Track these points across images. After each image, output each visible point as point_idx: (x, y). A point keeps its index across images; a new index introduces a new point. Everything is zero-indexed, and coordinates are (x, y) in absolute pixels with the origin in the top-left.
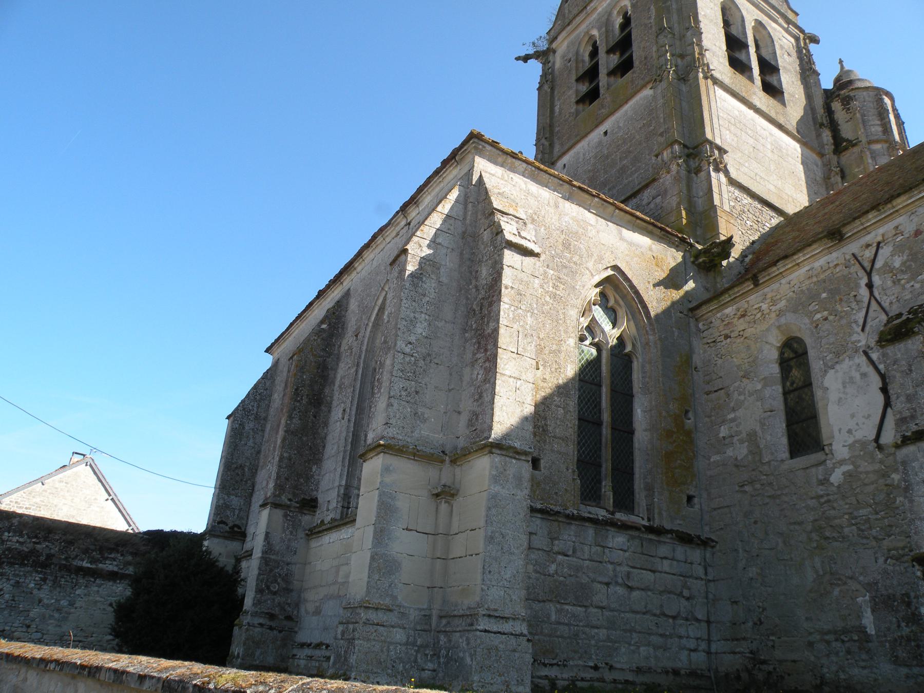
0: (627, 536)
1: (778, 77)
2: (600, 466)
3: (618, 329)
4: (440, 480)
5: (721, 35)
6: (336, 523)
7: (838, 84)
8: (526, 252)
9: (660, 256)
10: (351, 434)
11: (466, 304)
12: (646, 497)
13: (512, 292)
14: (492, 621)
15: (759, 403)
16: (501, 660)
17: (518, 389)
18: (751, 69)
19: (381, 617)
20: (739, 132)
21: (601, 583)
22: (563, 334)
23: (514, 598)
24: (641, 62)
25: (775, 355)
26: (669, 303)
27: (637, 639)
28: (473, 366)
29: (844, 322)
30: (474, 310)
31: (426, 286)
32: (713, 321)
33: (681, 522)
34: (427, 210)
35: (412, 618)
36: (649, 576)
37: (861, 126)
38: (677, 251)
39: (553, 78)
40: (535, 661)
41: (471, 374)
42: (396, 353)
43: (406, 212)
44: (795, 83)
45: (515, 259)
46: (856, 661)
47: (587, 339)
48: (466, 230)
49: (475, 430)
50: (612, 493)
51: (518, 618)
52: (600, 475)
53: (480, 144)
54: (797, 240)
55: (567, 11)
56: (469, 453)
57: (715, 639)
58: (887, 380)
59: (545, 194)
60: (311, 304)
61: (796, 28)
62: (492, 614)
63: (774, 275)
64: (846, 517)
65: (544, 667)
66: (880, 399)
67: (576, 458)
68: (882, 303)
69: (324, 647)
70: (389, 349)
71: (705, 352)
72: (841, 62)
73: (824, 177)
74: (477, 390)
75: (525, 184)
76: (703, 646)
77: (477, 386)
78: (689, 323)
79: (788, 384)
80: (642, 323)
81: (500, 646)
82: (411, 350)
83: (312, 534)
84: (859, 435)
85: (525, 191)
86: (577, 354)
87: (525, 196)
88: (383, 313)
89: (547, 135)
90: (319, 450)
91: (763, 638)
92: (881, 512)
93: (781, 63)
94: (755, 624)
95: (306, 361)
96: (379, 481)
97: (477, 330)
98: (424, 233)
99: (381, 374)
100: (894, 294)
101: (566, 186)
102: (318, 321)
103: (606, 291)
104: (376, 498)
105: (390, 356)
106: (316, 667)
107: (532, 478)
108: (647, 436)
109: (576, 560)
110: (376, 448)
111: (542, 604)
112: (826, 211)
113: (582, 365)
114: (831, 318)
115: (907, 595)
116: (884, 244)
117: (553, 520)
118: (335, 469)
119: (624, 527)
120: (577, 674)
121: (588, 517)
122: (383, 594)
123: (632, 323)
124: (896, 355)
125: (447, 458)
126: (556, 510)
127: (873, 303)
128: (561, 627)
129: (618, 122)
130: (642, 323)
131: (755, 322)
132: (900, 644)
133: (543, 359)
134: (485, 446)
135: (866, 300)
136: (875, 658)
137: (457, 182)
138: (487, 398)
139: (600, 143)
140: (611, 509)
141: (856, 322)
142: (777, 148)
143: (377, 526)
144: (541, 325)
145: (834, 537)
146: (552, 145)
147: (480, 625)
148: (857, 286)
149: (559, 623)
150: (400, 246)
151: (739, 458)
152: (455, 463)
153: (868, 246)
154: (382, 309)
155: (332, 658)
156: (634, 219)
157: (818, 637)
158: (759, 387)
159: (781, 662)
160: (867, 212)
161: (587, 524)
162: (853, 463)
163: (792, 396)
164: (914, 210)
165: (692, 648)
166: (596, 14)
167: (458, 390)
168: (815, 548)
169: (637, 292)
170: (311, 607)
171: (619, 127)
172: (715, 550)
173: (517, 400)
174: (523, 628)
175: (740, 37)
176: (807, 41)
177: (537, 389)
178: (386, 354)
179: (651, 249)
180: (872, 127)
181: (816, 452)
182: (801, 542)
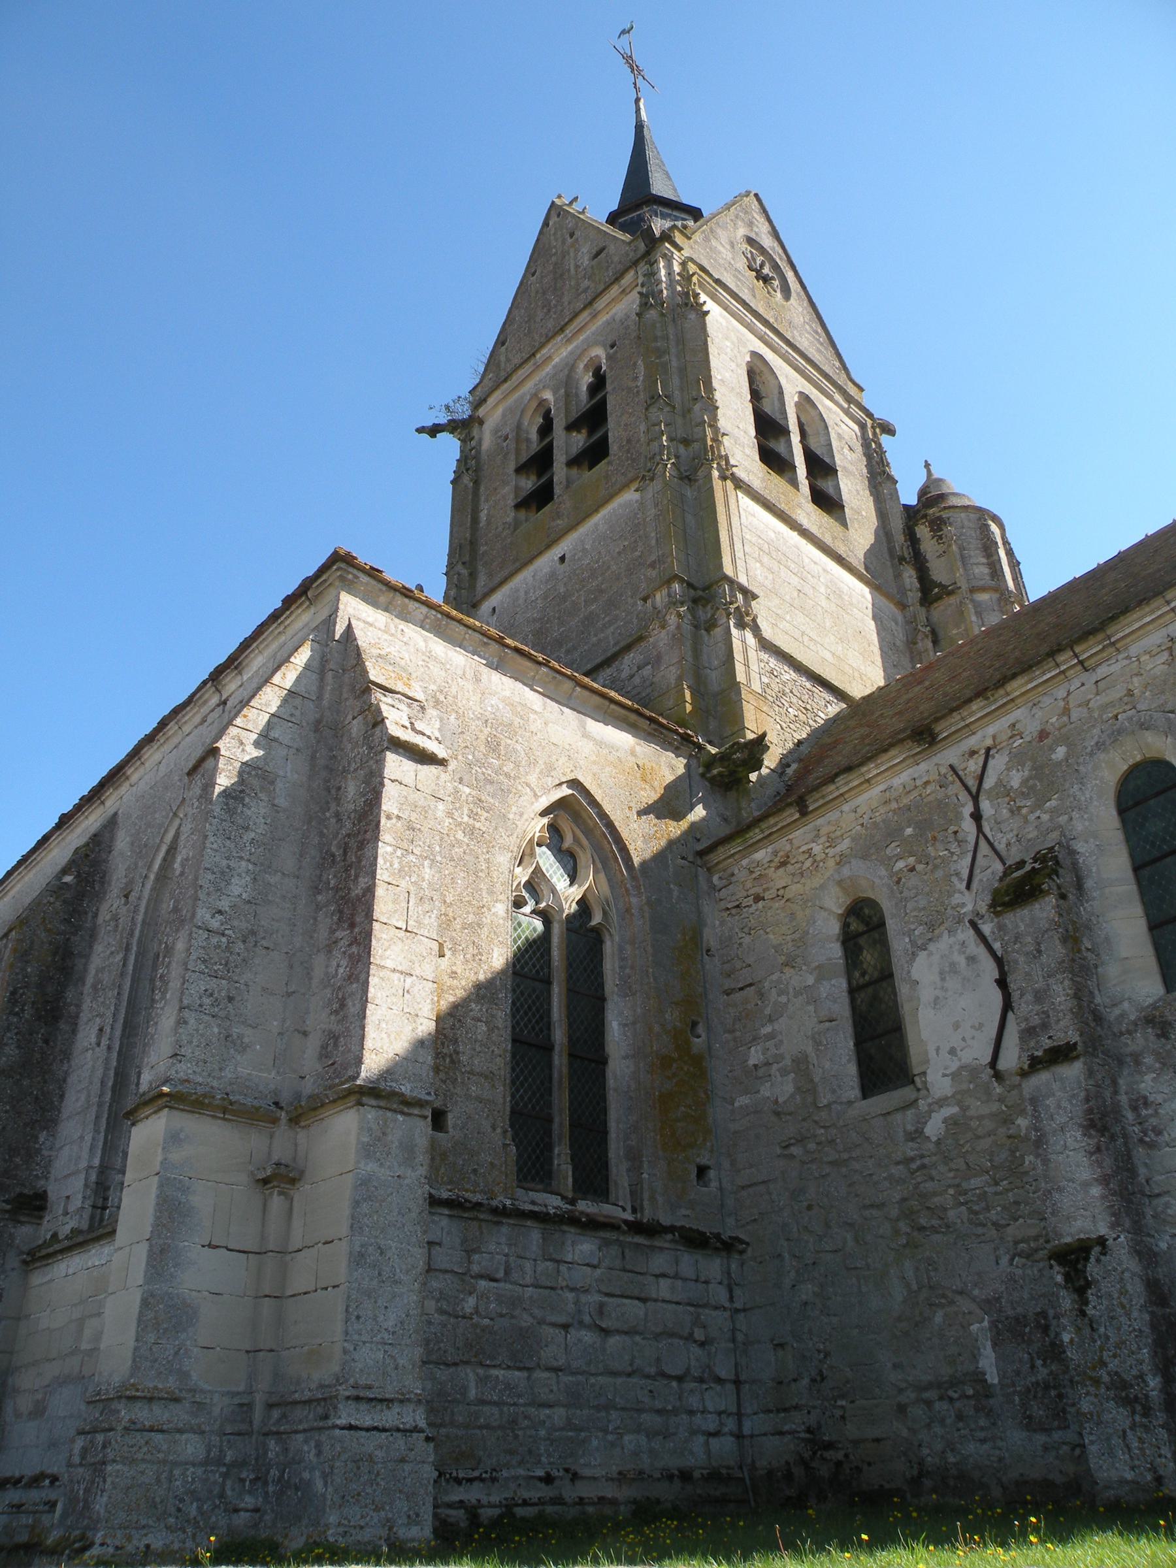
0: (597, 1241)
1: (835, 483)
2: (550, 1120)
3: (580, 886)
4: (269, 1154)
5: (747, 413)
6: (80, 1239)
7: (923, 499)
8: (424, 757)
9: (648, 765)
10: (112, 1073)
11: (319, 844)
12: (628, 1170)
13: (399, 824)
14: (362, 1408)
15: (811, 1008)
16: (379, 1480)
17: (408, 992)
18: (793, 468)
19: (158, 1414)
20: (775, 565)
21: (554, 1325)
22: (484, 894)
23: (401, 1362)
24: (621, 447)
25: (835, 928)
26: (663, 843)
27: (619, 1422)
28: (330, 952)
29: (939, 874)
30: (333, 855)
31: (249, 813)
32: (736, 872)
33: (688, 1212)
34: (256, 680)
35: (216, 1411)
36: (634, 1309)
37: (959, 564)
38: (677, 756)
39: (478, 462)
40: (440, 1475)
41: (327, 967)
42: (194, 929)
43: (219, 683)
44: (861, 493)
45: (405, 769)
46: (971, 1430)
47: (526, 903)
48: (322, 716)
49: (333, 1064)
50: (570, 1167)
51: (409, 1400)
52: (550, 1137)
53: (349, 573)
54: (867, 741)
55: (503, 359)
56: (322, 1105)
57: (749, 1411)
58: (1006, 968)
59: (458, 659)
60: (45, 839)
61: (860, 410)
62: (361, 1395)
63: (831, 797)
64: (951, 1191)
65: (456, 1486)
66: (997, 996)
67: (508, 1109)
68: (996, 844)
69: (47, 1482)
70: (183, 922)
71: (722, 923)
72: (927, 465)
73: (907, 641)
74: (337, 995)
75: (425, 641)
76: (730, 1424)
77: (336, 987)
78: (696, 876)
79: (857, 974)
80: (619, 876)
81: (376, 1453)
82: (222, 924)
83: (34, 1260)
84: (967, 1057)
85: (423, 654)
86: (510, 929)
87: (424, 661)
88: (174, 857)
89: (467, 558)
90: (52, 1102)
91: (826, 1404)
92: (1002, 1181)
93: (839, 461)
94: (813, 1380)
95: (32, 943)
96: (160, 1158)
97: (337, 889)
98: (248, 721)
99: (167, 967)
100: (1012, 831)
101: (494, 646)
102: (59, 868)
103: (560, 822)
104: (154, 1191)
105: (183, 934)
106: (27, 1526)
107: (433, 1146)
108: (628, 1067)
109: (510, 1286)
110: (156, 1100)
111: (452, 1370)
112: (911, 695)
113: (518, 947)
114: (920, 867)
115: (1043, 1314)
116: (995, 750)
117: (470, 1219)
118: (82, 1138)
119: (592, 1225)
120: (515, 1492)
121: (531, 1212)
122: (162, 1369)
123: (602, 876)
124: (1017, 926)
125: (283, 1114)
126: (474, 1200)
127: (983, 843)
128: (486, 1409)
129: (582, 541)
130: (619, 876)
131: (802, 874)
132: (1035, 1397)
133: (452, 939)
134: (350, 1092)
135: (972, 839)
136: (1000, 1423)
137: (309, 635)
138: (352, 1009)
139: (553, 575)
140: (570, 1195)
141: (957, 874)
142: (835, 593)
143: (154, 1242)
144: (448, 880)
145: (933, 1226)
146: (473, 575)
147: (340, 1417)
148: (959, 817)
149: (483, 1402)
150: (208, 741)
151: (781, 1100)
152: (297, 1123)
153: (973, 753)
154: (172, 849)
155: (59, 1507)
156: (607, 703)
157: (913, 1396)
158: (810, 980)
159: (856, 1443)
160: (969, 701)
161: (529, 1223)
162: (959, 1103)
163: (863, 995)
164: (1037, 700)
165: (712, 1430)
166: (550, 367)
167: (304, 994)
168: (904, 1246)
169: (610, 825)
170: (24, 1403)
171: (584, 550)
172: (745, 1257)
173: (405, 1011)
174: (418, 1418)
175: (777, 417)
176: (878, 430)
177: (440, 991)
178: (177, 930)
179: (633, 753)
180: (975, 567)
181: (903, 1086)
182: (882, 1237)
